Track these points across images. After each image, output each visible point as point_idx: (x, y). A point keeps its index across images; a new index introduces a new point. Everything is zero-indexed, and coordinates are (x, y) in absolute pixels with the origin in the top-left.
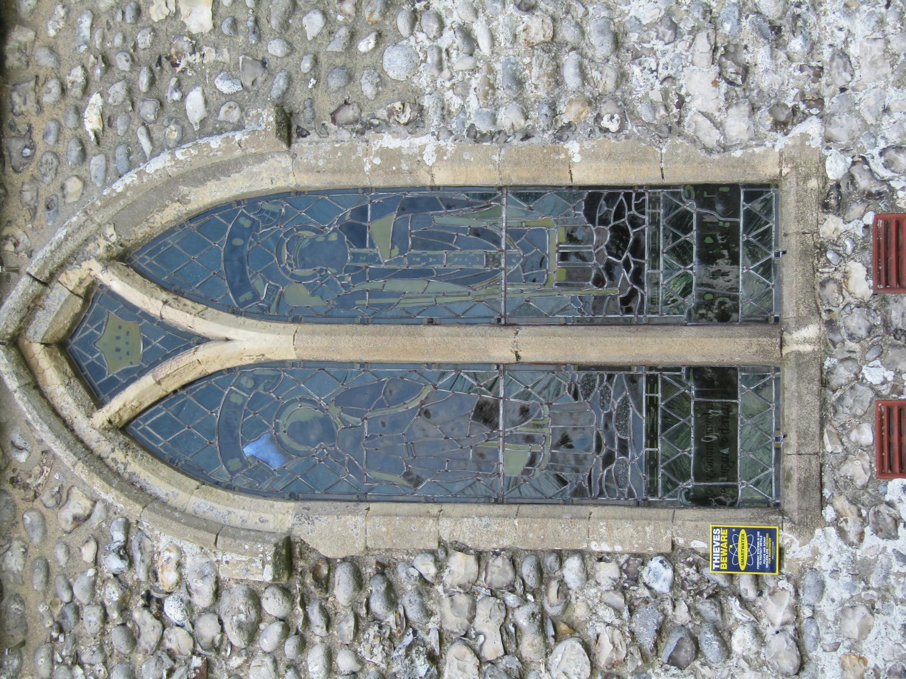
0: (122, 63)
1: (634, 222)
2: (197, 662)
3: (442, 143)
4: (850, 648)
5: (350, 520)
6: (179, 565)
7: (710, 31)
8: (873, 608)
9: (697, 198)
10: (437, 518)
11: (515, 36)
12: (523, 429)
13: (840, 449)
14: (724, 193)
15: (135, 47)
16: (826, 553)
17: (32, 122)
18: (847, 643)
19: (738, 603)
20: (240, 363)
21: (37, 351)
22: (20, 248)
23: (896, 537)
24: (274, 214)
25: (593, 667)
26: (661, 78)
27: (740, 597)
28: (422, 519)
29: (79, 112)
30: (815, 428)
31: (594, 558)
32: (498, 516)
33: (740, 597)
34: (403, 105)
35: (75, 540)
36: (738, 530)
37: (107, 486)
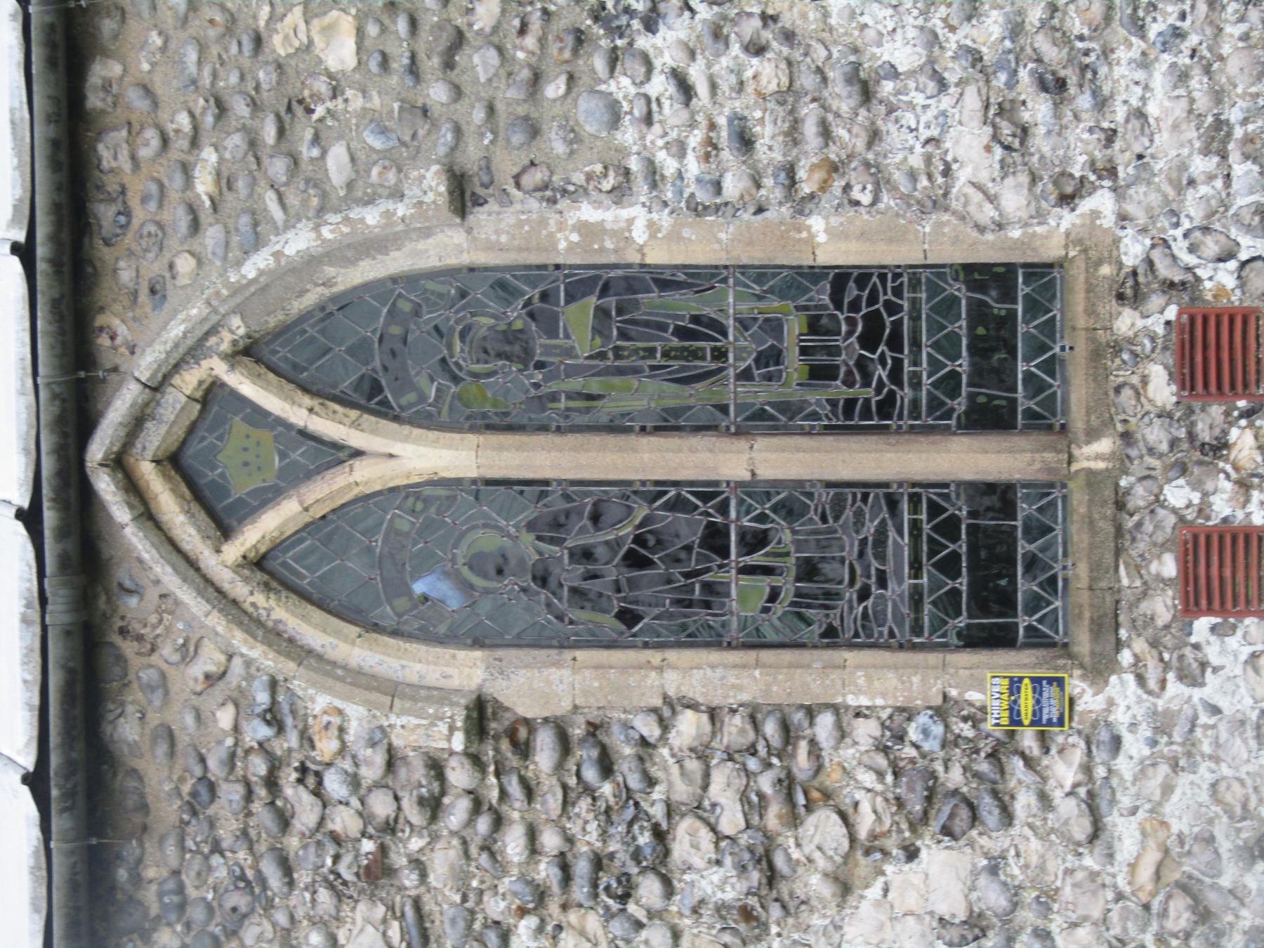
0: (240, 108)
1: (892, 308)
2: (368, 846)
3: (655, 216)
4: (1152, 811)
5: (554, 674)
6: (342, 730)
7: (981, 84)
8: (1177, 765)
9: (966, 282)
10: (660, 669)
11: (741, 83)
12: (756, 559)
13: (1138, 583)
14: (997, 275)
15: (257, 88)
16: (1122, 704)
17: (125, 181)
18: (1148, 806)
19: (1021, 763)
20: (405, 482)
21: (147, 471)
22: (119, 341)
23: (1202, 684)
24: (441, 296)
25: (853, 839)
26: (923, 138)
27: (1023, 755)
28: (643, 672)
29: (186, 169)
30: (1109, 558)
31: (851, 713)
32: (735, 666)
33: (1023, 755)
34: (606, 168)
35: (208, 703)
36: (1021, 679)
37: (250, 640)
